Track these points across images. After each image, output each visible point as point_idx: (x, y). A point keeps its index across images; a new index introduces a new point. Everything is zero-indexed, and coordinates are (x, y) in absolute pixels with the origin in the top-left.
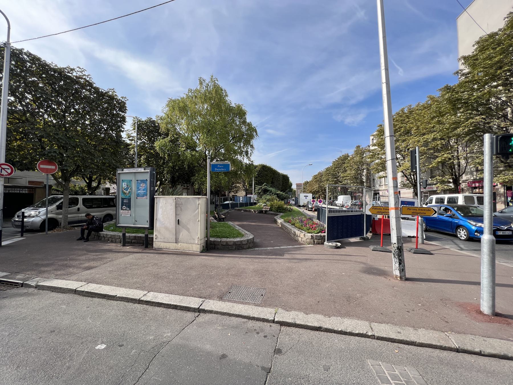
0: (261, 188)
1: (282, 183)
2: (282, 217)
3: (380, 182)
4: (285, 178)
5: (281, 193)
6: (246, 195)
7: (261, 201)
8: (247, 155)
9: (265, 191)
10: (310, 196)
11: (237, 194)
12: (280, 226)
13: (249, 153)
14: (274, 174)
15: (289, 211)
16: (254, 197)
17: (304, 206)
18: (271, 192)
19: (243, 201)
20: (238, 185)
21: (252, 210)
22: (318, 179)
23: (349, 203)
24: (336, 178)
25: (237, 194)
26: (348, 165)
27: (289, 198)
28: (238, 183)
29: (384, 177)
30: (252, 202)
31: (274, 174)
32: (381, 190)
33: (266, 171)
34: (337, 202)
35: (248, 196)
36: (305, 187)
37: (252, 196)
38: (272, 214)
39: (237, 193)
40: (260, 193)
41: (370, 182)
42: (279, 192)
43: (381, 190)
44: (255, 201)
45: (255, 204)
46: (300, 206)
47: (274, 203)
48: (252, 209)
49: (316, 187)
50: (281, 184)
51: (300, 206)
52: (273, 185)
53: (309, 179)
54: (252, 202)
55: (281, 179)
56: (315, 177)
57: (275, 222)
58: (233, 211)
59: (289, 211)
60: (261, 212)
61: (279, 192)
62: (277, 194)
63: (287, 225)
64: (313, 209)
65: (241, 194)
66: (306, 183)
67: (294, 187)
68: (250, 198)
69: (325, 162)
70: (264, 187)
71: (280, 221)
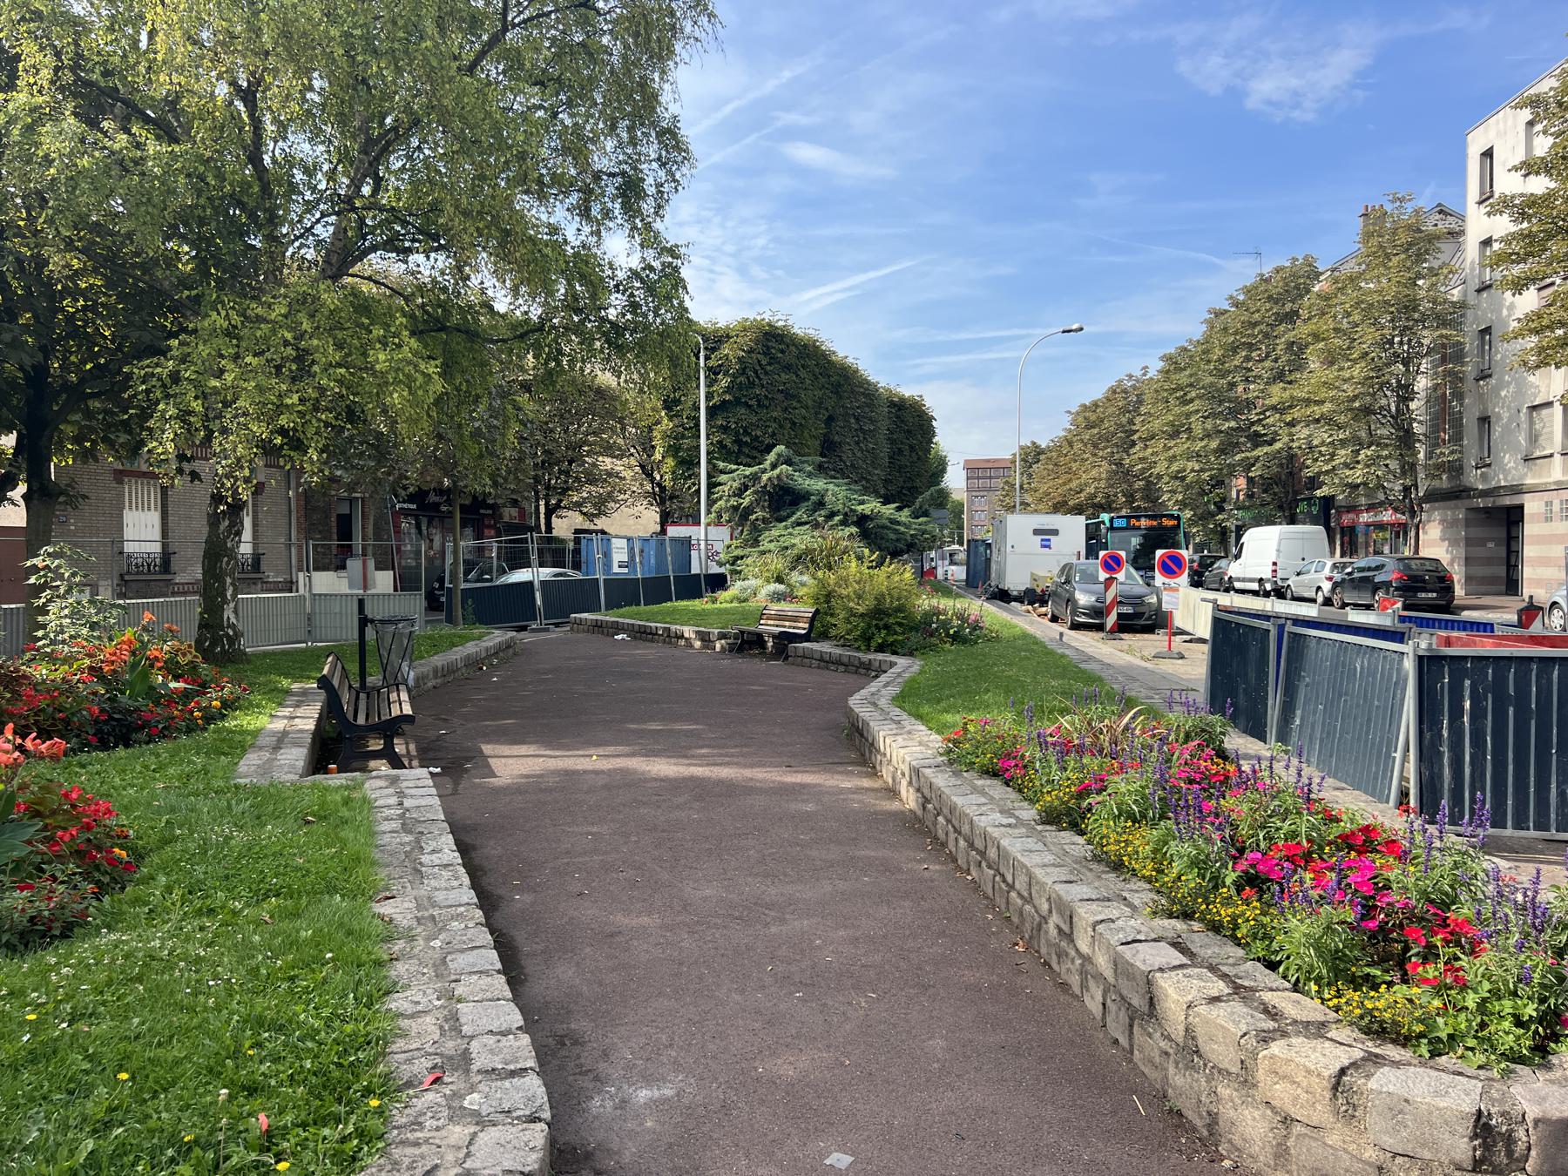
0: (755, 478)
1: (888, 447)
2: (911, 699)
3: (1534, 438)
4: (911, 423)
5: (888, 510)
6: (663, 531)
7: (751, 564)
8: (631, 211)
9: (783, 501)
10: (1073, 528)
11: (601, 523)
12: (909, 799)
13: (649, 186)
14: (837, 389)
15: (957, 638)
16: (708, 539)
17: (1033, 597)
18: (821, 504)
19: (629, 564)
20: (607, 463)
21: (688, 632)
22: (1111, 425)
23: (1321, 573)
24: (1234, 413)
25: (601, 523)
26: (1326, 325)
27: (933, 542)
28: (609, 450)
29: (212, 596)
30: (695, 570)
31: (837, 389)
32: (1533, 490)
33: (788, 368)
34: (1234, 569)
35: (673, 531)
36: (1031, 476)
37: (697, 533)
38: (826, 662)
39: (601, 513)
40: (748, 511)
41: (1457, 438)
42: (871, 506)
43: (1533, 490)
44: (715, 569)
45: (718, 582)
46: (1003, 596)
47: (845, 581)
48: (688, 620)
49: (1094, 476)
50: (884, 452)
51: (1003, 596)
52: (831, 459)
53: (1049, 430)
54: (695, 570)
55: (884, 425)
56: (1089, 417)
57: (856, 746)
58: (555, 634)
59: (957, 638)
60: (748, 643)
61: (871, 506)
62: (862, 521)
63: (986, 809)
64: (1111, 620)
65: (630, 524)
66: (1032, 456)
67: (955, 481)
68: (686, 544)
69: (1152, 326)
70: (772, 468)
71: (907, 747)
